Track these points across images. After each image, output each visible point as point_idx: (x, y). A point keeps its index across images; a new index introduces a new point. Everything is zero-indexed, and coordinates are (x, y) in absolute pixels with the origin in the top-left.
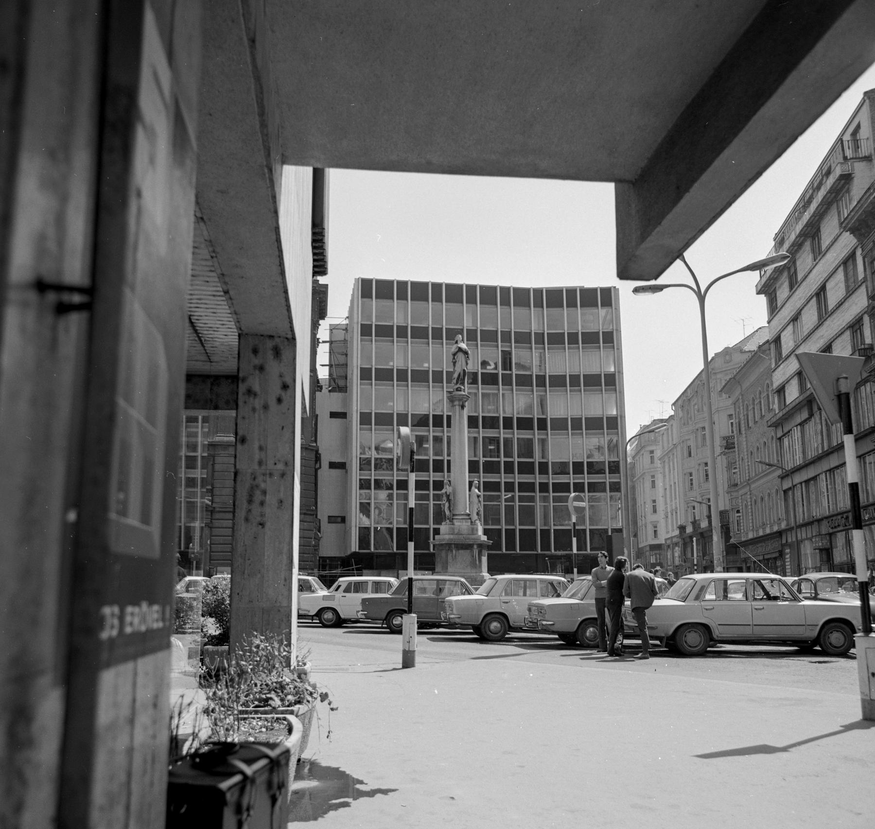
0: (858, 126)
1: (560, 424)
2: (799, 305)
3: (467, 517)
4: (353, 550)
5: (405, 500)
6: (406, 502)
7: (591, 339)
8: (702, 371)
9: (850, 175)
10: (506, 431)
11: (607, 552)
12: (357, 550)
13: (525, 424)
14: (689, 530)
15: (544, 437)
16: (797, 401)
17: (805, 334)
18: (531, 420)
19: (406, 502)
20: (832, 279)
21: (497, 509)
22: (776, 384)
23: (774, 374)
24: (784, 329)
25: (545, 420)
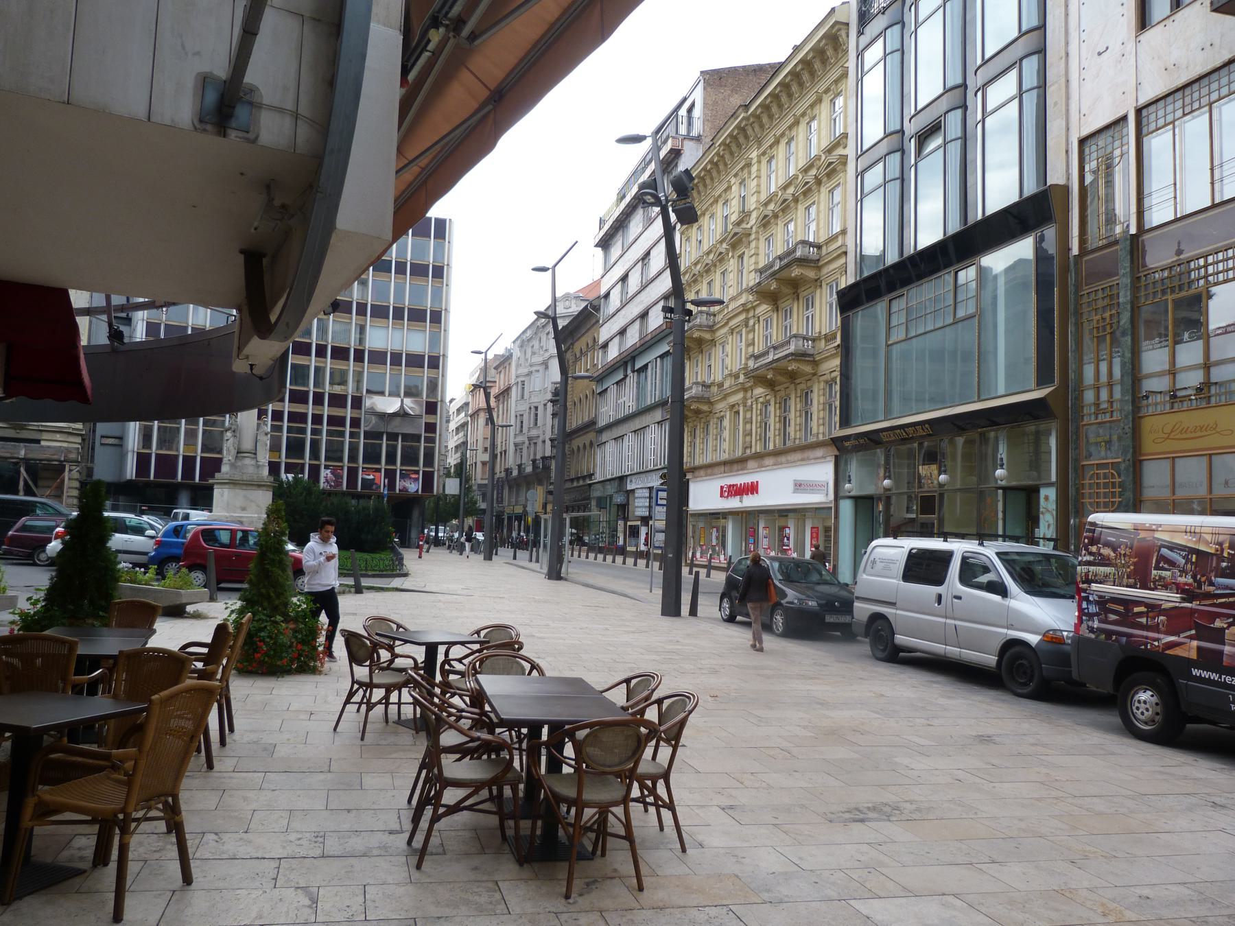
0: (693, 105)
1: (378, 357)
2: (627, 267)
3: (253, 456)
4: (128, 477)
5: (389, 392)
6: (387, 393)
7: (417, 316)
8: (550, 306)
9: (680, 150)
10: (318, 359)
11: (408, 231)
12: (134, 478)
13: (340, 353)
14: (515, 473)
15: (360, 369)
16: (618, 359)
17: (629, 296)
18: (347, 350)
19: (387, 393)
20: (655, 247)
21: (302, 443)
22: (602, 340)
23: (601, 329)
24: (613, 287)
25: (362, 352)
